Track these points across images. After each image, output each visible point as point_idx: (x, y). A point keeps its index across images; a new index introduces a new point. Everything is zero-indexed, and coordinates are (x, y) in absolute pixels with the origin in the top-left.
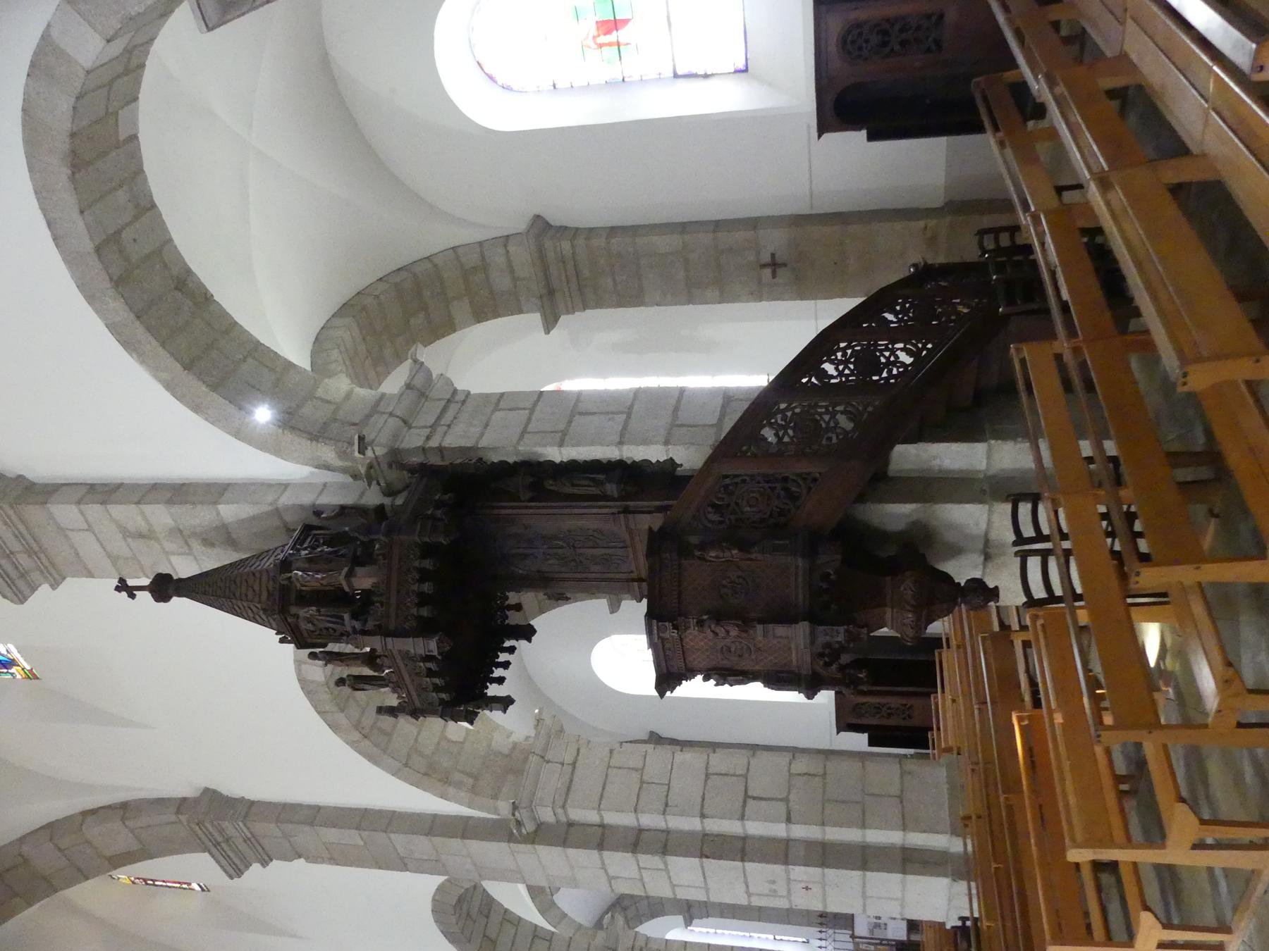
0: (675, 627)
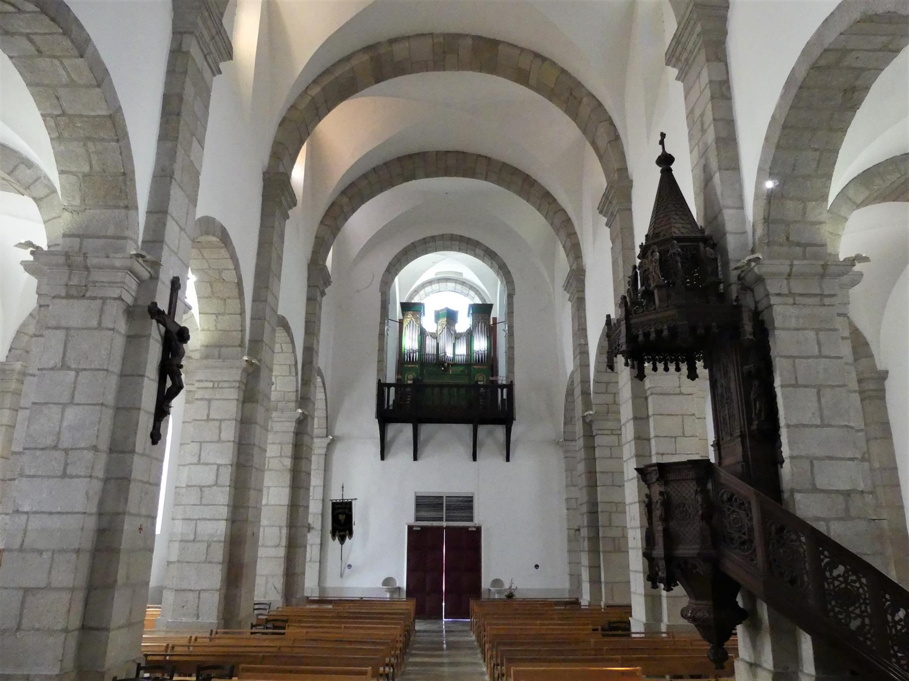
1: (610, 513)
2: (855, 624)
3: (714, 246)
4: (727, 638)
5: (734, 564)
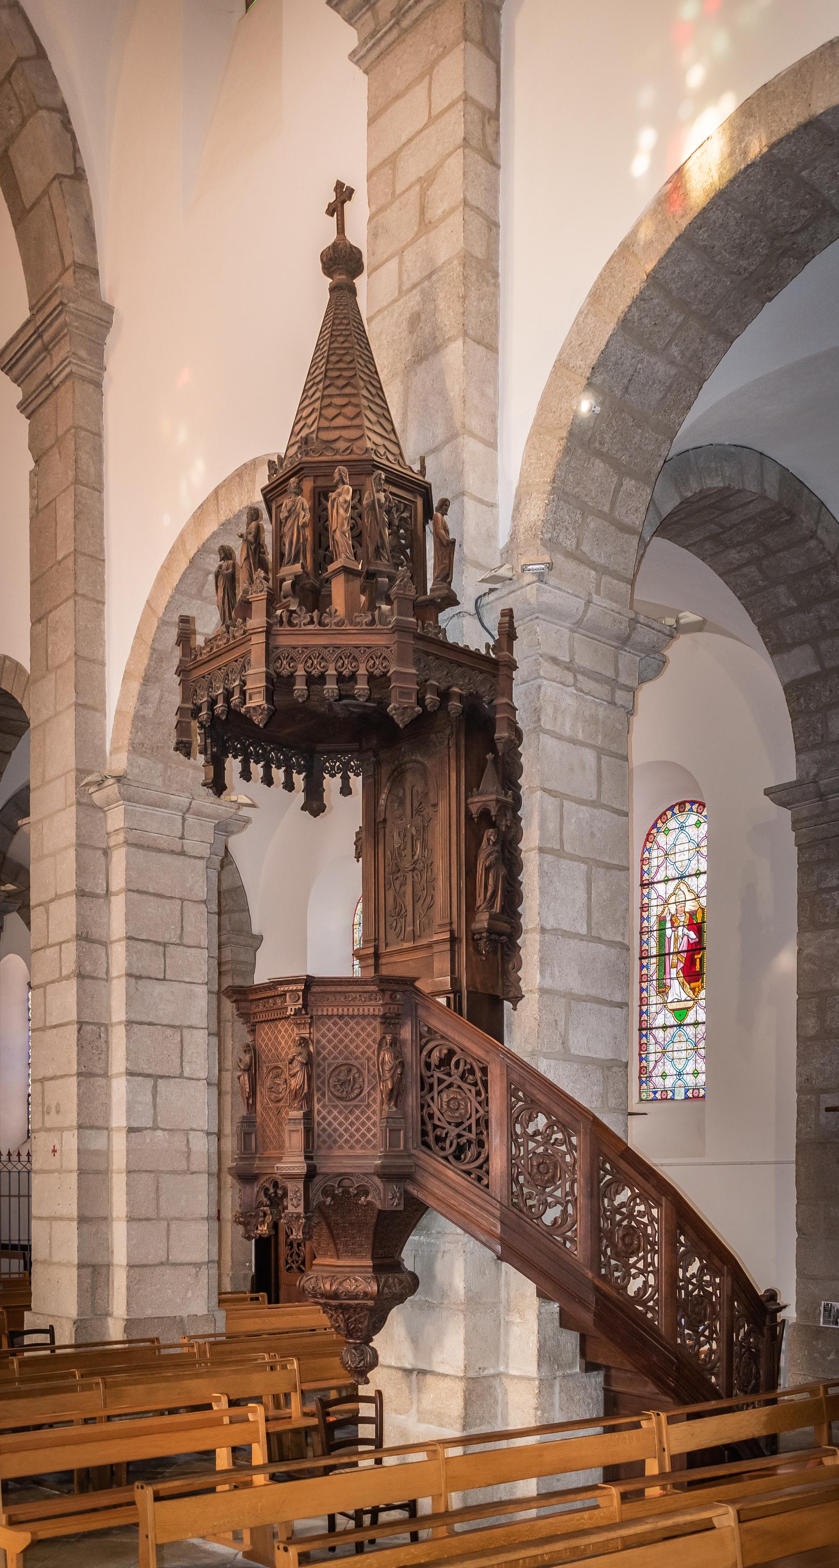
0: (297, 1012)
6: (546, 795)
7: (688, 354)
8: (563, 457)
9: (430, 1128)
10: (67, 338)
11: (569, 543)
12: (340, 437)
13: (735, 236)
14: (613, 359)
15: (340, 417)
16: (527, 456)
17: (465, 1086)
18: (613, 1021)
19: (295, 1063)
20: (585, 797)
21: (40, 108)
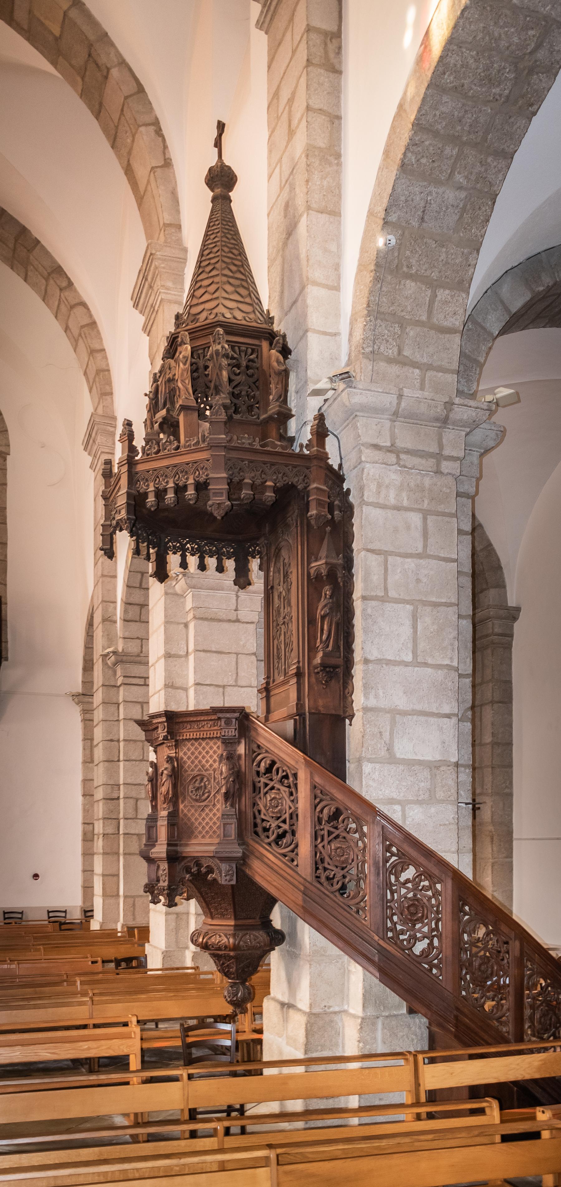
1: (137, 800)
2: (419, 947)
3: (286, 352)
4: (255, 970)
5: (267, 869)
6: (369, 554)
7: (473, 177)
8: (374, 285)
9: (258, 821)
10: (159, 277)
11: (390, 351)
12: (204, 309)
13: (479, 71)
14: (403, 198)
15: (206, 295)
16: (355, 291)
17: (282, 788)
18: (441, 729)
19: (164, 775)
20: (410, 551)
21: (139, 126)
